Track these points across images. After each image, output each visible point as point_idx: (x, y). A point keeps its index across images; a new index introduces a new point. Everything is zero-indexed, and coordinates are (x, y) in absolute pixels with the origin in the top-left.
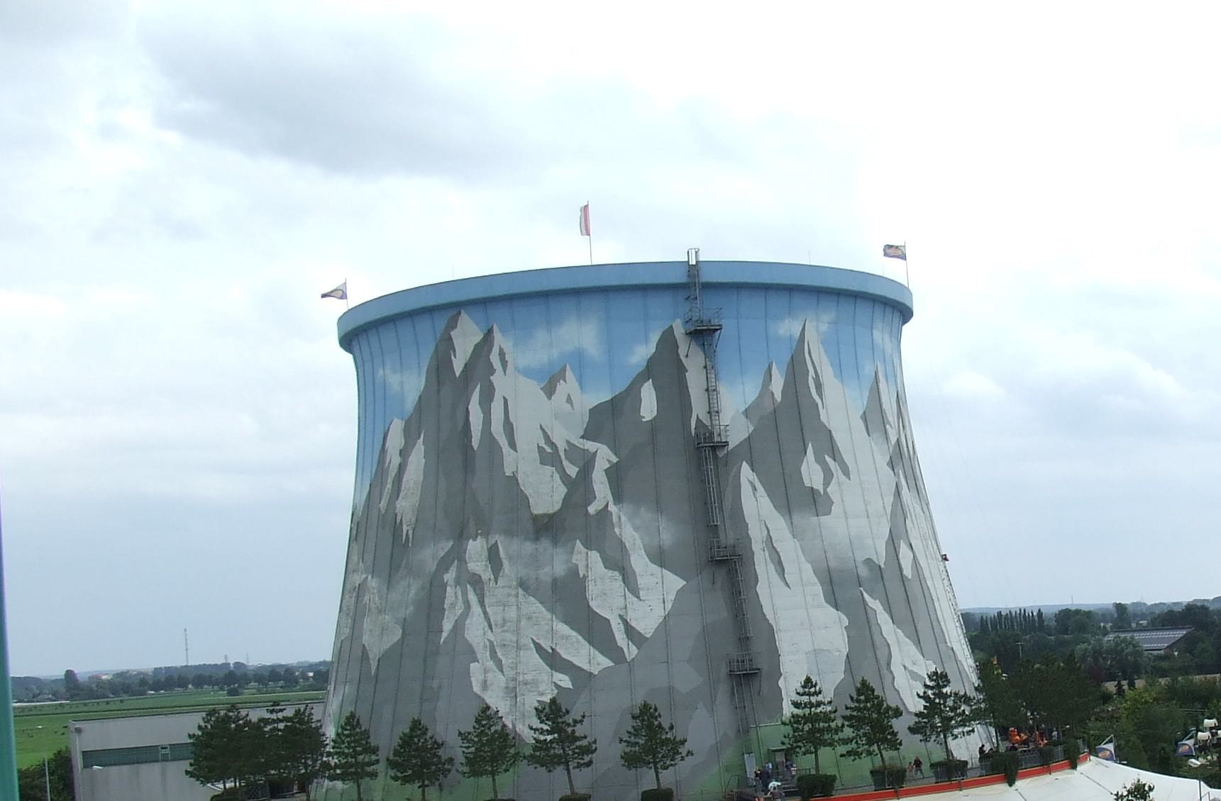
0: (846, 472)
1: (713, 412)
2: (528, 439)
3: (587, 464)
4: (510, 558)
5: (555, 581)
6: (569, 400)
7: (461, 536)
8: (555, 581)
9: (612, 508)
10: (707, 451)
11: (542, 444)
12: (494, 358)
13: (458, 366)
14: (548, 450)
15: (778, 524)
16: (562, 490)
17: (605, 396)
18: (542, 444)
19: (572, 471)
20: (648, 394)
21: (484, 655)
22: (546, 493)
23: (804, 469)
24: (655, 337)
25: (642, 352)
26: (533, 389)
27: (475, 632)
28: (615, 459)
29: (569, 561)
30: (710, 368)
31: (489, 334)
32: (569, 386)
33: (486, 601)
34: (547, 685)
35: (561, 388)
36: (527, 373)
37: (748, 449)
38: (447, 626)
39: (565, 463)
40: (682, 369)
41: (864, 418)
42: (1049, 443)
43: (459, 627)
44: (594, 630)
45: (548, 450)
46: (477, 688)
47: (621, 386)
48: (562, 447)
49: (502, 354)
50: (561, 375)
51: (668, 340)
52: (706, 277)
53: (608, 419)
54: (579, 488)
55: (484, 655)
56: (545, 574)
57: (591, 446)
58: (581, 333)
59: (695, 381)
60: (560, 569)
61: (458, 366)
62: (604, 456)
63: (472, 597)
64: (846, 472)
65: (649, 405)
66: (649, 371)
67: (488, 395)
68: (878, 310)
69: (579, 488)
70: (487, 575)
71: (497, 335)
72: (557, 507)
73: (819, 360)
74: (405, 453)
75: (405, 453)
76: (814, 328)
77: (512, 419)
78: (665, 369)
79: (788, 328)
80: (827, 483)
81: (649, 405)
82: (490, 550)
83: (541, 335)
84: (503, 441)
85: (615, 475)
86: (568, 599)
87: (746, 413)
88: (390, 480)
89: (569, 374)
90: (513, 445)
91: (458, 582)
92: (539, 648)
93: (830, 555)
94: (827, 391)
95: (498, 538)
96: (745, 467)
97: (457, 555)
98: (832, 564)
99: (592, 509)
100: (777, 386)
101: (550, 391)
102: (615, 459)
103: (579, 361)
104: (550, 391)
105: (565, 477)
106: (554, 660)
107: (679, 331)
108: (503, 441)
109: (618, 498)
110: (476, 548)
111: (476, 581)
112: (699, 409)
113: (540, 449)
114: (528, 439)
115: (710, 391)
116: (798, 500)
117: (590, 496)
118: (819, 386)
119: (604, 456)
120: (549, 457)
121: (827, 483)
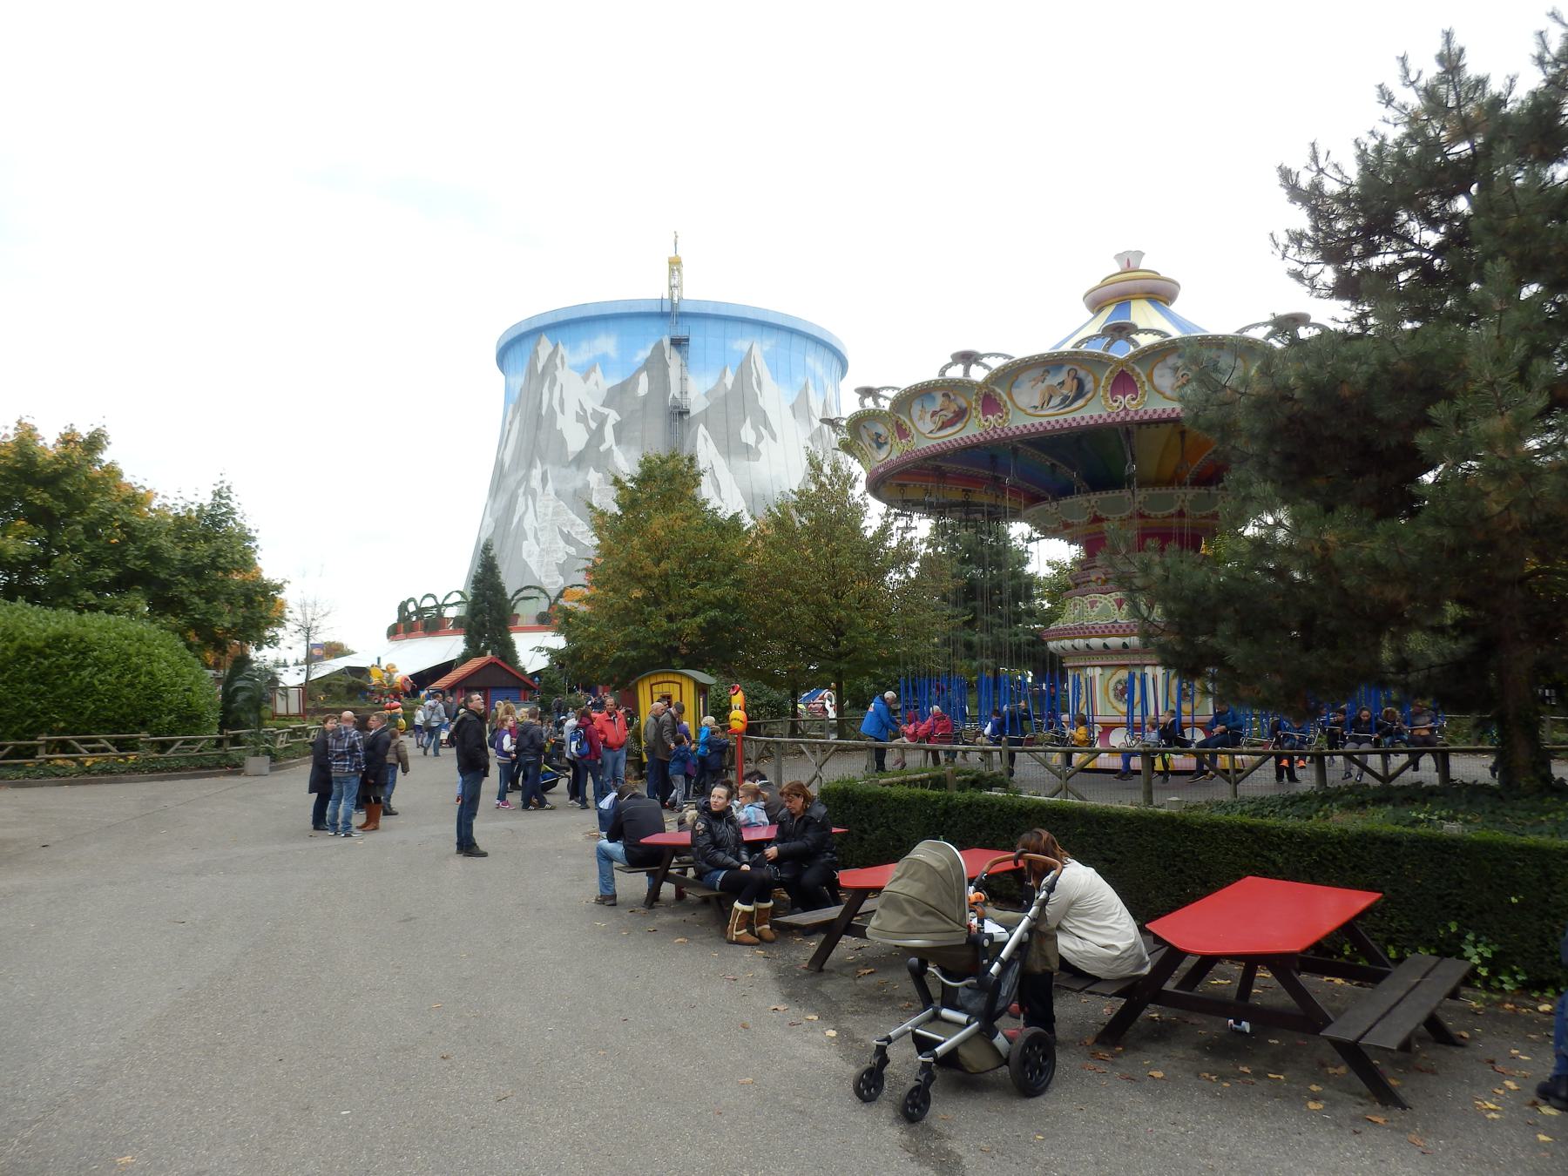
0: (774, 438)
1: (684, 392)
9: (614, 448)
12: (558, 361)
15: (720, 464)
16: (587, 437)
17: (618, 381)
19: (593, 425)
21: (530, 535)
23: (742, 432)
24: (651, 346)
25: (643, 355)
26: (577, 376)
27: (529, 523)
30: (684, 366)
31: (556, 346)
32: (597, 375)
35: (593, 377)
36: (574, 368)
37: (705, 416)
38: (516, 520)
40: (666, 366)
41: (793, 407)
43: (521, 520)
46: (524, 556)
47: (627, 376)
48: (589, 411)
51: (659, 347)
52: (684, 308)
53: (615, 397)
54: (596, 436)
55: (530, 535)
57: (606, 411)
58: (606, 343)
59: (674, 373)
60: (579, 483)
62: (613, 417)
64: (774, 438)
65: (643, 386)
66: (647, 366)
67: (554, 381)
68: (810, 345)
69: (596, 436)
71: (561, 347)
73: (761, 366)
76: (760, 349)
78: (656, 366)
79: (741, 345)
80: (758, 442)
81: (643, 386)
83: (584, 345)
84: (557, 409)
85: (619, 429)
87: (706, 394)
89: (598, 369)
90: (563, 412)
91: (525, 494)
92: (561, 531)
93: (775, 510)
94: (765, 392)
95: (548, 467)
96: (702, 429)
97: (527, 478)
98: (756, 491)
100: (729, 380)
101: (586, 378)
103: (604, 360)
104: (586, 378)
107: (667, 342)
108: (557, 409)
109: (618, 441)
110: (536, 473)
111: (533, 494)
112: (675, 390)
114: (572, 407)
115: (683, 380)
116: (733, 448)
117: (602, 440)
118: (759, 384)
120: (582, 418)
121: (758, 442)
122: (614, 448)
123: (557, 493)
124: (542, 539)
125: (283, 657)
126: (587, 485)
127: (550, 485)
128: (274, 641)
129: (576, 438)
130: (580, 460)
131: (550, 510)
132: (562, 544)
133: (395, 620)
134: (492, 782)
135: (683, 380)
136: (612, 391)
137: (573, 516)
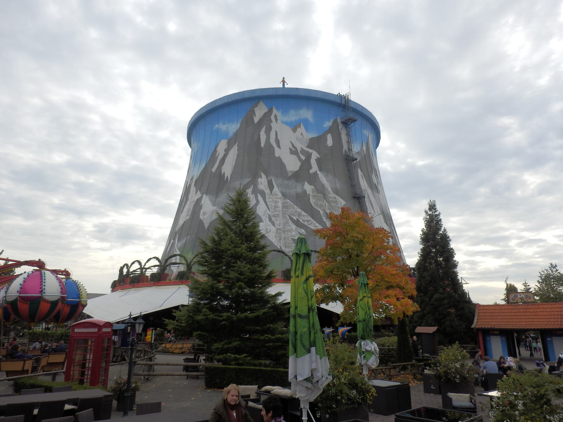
1: (350, 150)
2: (286, 145)
3: (309, 156)
4: (278, 186)
5: (297, 194)
6: (302, 134)
7: (255, 176)
8: (297, 194)
9: (318, 172)
10: (349, 160)
11: (291, 147)
13: (256, 120)
14: (293, 149)
16: (299, 164)
17: (315, 135)
18: (291, 147)
20: (329, 138)
21: (265, 219)
22: (292, 164)
24: (332, 121)
25: (328, 124)
26: (288, 130)
28: (319, 156)
29: (303, 188)
33: (267, 200)
34: (295, 232)
35: (299, 130)
36: (286, 123)
39: (301, 155)
40: (340, 134)
42: (562, 270)
44: (313, 213)
45: (293, 149)
48: (299, 150)
49: (276, 116)
50: (299, 126)
51: (335, 121)
54: (306, 164)
56: (293, 192)
57: (310, 151)
58: (307, 114)
59: (344, 138)
60: (299, 190)
61: (256, 120)
62: (315, 155)
63: (260, 198)
65: (330, 141)
66: (330, 130)
69: (306, 164)
70: (267, 191)
71: (275, 111)
72: (298, 169)
74: (227, 151)
75: (227, 151)
77: (279, 137)
78: (334, 130)
81: (330, 141)
82: (268, 182)
83: (292, 112)
84: (275, 145)
86: (302, 200)
88: (240, 367)
89: (302, 126)
90: (279, 147)
97: (254, 182)
99: (311, 171)
101: (294, 130)
102: (319, 156)
103: (305, 122)
104: (294, 130)
105: (300, 159)
106: (298, 223)
107: (339, 121)
108: (275, 145)
112: (345, 147)
113: (290, 149)
114: (286, 145)
119: (315, 155)
120: (294, 151)
122: (318, 172)
123: (283, 194)
124: (276, 223)
125: (519, 291)
126: (305, 192)
127: (276, 189)
128: (95, 226)
129: (292, 164)
130: (297, 176)
131: (280, 204)
132: (294, 227)
133: (116, 278)
134: (152, 373)
135: (348, 142)
136: (311, 140)
137: (299, 210)
